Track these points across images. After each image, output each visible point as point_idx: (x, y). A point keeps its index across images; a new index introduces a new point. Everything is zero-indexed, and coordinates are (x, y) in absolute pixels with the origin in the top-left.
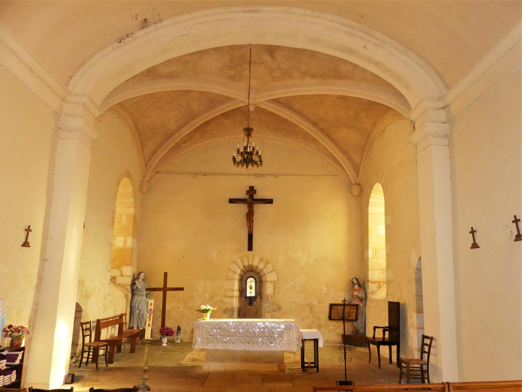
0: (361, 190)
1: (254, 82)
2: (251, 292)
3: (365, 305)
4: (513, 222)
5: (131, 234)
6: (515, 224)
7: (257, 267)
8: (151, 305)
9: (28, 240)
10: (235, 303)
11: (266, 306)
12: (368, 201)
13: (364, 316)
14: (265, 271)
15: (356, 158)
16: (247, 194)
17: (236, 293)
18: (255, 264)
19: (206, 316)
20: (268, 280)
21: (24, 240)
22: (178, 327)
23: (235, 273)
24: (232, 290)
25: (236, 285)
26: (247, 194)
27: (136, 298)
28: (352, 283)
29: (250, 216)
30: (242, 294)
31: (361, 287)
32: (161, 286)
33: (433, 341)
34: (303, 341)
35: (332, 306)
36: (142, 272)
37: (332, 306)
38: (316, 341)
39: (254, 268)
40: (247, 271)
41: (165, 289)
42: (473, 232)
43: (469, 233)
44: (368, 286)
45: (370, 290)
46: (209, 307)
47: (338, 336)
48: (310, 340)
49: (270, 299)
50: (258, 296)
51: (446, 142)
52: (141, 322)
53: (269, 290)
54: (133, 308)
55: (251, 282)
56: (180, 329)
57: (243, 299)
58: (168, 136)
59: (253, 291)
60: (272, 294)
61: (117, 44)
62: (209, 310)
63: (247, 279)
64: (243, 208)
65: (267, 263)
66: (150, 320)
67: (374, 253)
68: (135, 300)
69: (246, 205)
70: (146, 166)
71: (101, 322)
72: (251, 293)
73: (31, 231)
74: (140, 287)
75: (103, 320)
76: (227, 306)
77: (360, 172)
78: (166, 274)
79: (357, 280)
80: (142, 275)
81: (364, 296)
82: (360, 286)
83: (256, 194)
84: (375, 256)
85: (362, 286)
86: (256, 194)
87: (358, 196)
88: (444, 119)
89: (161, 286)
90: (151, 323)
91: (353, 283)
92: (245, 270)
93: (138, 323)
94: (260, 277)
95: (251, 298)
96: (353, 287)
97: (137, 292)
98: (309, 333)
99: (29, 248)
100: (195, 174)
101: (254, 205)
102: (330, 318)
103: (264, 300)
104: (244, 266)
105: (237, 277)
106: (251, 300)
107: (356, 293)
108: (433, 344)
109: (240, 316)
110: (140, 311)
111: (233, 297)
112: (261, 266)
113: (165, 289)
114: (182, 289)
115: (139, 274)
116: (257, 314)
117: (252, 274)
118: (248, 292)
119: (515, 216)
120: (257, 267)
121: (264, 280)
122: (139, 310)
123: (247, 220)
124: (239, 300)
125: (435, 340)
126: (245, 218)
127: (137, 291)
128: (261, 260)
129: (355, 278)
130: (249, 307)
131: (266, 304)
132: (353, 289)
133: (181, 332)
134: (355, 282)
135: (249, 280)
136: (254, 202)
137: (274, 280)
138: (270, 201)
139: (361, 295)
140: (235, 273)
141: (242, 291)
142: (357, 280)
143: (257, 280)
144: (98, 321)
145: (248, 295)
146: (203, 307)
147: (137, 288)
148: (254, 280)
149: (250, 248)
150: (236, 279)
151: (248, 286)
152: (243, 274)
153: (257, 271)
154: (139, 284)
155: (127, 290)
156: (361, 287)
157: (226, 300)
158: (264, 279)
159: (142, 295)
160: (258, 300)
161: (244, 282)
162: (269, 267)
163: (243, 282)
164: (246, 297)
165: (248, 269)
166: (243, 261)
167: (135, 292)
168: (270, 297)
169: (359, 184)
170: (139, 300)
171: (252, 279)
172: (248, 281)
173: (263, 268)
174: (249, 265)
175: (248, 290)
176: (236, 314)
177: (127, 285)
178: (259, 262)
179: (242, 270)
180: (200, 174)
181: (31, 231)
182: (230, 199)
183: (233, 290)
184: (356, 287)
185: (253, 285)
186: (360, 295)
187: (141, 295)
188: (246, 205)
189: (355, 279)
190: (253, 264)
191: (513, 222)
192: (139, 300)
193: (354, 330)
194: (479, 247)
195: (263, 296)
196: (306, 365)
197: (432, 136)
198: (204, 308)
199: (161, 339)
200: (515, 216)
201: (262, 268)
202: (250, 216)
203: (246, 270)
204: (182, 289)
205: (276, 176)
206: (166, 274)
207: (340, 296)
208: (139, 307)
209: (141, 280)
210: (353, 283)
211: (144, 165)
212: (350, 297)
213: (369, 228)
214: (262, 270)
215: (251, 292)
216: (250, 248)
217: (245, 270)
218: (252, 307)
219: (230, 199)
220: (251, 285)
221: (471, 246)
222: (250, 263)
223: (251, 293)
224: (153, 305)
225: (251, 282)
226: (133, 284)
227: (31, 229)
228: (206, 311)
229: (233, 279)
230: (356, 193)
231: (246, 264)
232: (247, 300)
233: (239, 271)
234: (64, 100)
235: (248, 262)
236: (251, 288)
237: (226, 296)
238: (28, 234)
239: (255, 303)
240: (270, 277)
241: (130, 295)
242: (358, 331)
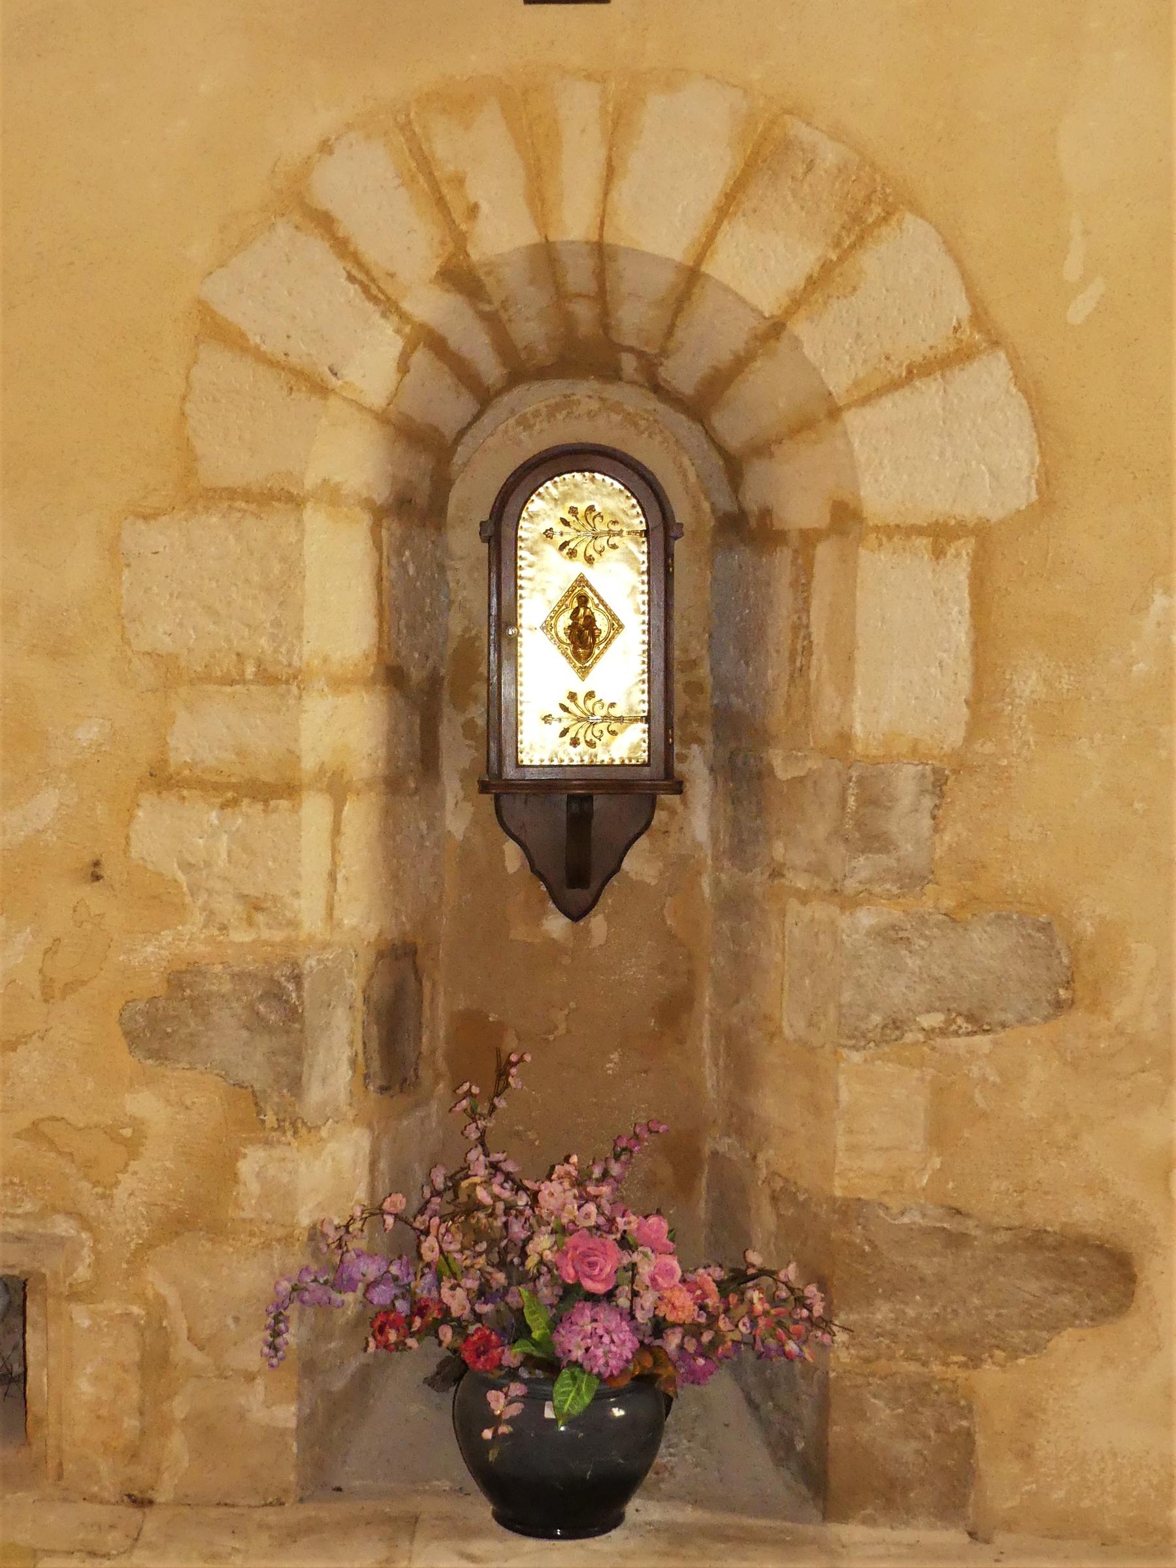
24: (268, 678)
130: (556, 924)
143: (682, 512)
150: (331, 495)
172: (528, 530)
201: (769, 303)
203: (503, 345)
218: (597, 923)
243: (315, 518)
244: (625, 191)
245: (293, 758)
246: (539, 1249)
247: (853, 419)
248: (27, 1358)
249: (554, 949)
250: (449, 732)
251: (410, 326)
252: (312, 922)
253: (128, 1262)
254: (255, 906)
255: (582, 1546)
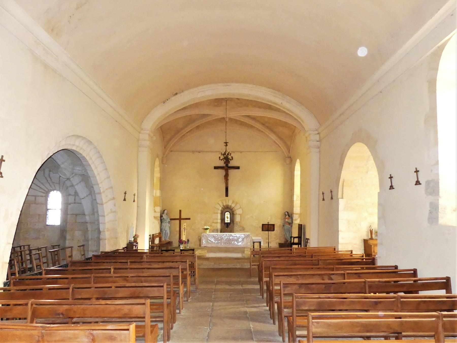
0: (291, 160)
1: (228, 107)
2: (227, 220)
3: (292, 227)
4: (389, 178)
5: (159, 188)
6: (390, 179)
7: (231, 206)
8: (185, 226)
9: (126, 198)
10: (219, 226)
11: (236, 228)
12: (295, 167)
13: (291, 233)
14: (236, 208)
15: (289, 143)
16: (224, 164)
17: (219, 221)
18: (230, 204)
19: (207, 231)
20: (237, 213)
21: (124, 198)
22: (188, 240)
23: (219, 209)
24: (217, 219)
25: (219, 216)
26: (224, 164)
27: (163, 224)
28: (285, 215)
29: (226, 177)
30: (222, 221)
31: (290, 217)
32: (178, 217)
33: (309, 240)
34: (254, 243)
35: (263, 225)
36: (165, 210)
37: (263, 225)
38: (260, 243)
39: (229, 207)
40: (225, 208)
41: (180, 219)
42: (417, 171)
43: (414, 172)
44: (293, 216)
45: (294, 219)
46: (208, 227)
47: (277, 244)
48: (257, 242)
49: (238, 224)
50: (232, 222)
51: (318, 150)
52: (167, 237)
53: (238, 219)
54: (162, 229)
55: (227, 215)
56: (189, 241)
57: (223, 224)
58: (178, 131)
59: (229, 220)
60: (240, 221)
61: (162, 104)
62: (208, 228)
63: (225, 213)
64: (222, 172)
65: (237, 204)
66: (185, 232)
67: (297, 198)
68: (163, 226)
69: (224, 170)
70: (165, 148)
71: (155, 235)
72: (227, 220)
73: (4, 161)
74: (165, 218)
75: (155, 234)
76: (214, 228)
77: (291, 150)
78: (180, 211)
79: (288, 213)
80: (166, 211)
81: (291, 222)
82: (289, 216)
83: (229, 163)
84: (297, 199)
85: (291, 216)
86: (229, 163)
87: (289, 164)
88: (318, 139)
89: (178, 217)
90: (185, 233)
91: (285, 214)
92: (224, 208)
93: (165, 238)
94: (233, 212)
95: (227, 223)
96: (286, 216)
97: (164, 221)
98: (256, 239)
99: (2, 178)
100: (193, 152)
101: (229, 170)
102: (263, 230)
103: (235, 225)
104: (223, 206)
105: (220, 212)
106: (228, 225)
107: (287, 220)
108: (308, 241)
109: (221, 232)
110: (166, 231)
111: (217, 223)
112: (233, 205)
113: (180, 219)
114: (189, 219)
115: (164, 211)
116: (232, 231)
117: (228, 210)
118: (226, 220)
119: (390, 175)
120: (231, 206)
121: (235, 213)
122: (165, 231)
123: (225, 179)
124: (221, 224)
125: (309, 240)
126: (224, 178)
127: (164, 220)
128: (233, 202)
129: (287, 212)
130: (227, 228)
131: (236, 226)
132: (285, 218)
133: (189, 242)
134: (287, 214)
135: (226, 213)
136: (229, 169)
137: (240, 213)
138: (238, 168)
139: (290, 221)
140: (219, 209)
141: (223, 219)
142: (288, 213)
143: (231, 213)
144: (153, 235)
145: (226, 222)
146: (206, 227)
147: (164, 218)
148: (229, 213)
149: (227, 195)
150: (219, 213)
151: (226, 217)
152: (223, 210)
153: (231, 209)
154: (164, 216)
155: (158, 220)
156: (290, 217)
157: (213, 225)
158: (235, 213)
159: (167, 222)
160: (232, 224)
161: (223, 214)
162: (238, 206)
163: (223, 214)
164: (225, 223)
165: (226, 207)
166: (222, 203)
167: (162, 221)
168: (238, 222)
169: (290, 157)
170: (165, 226)
171: (228, 213)
172: (225, 214)
173: (234, 206)
174: (226, 205)
175: (226, 219)
176: (219, 231)
177: (158, 217)
178: (232, 203)
179: (222, 208)
180: (197, 151)
181: (4, 161)
182: (214, 167)
183: (217, 219)
184: (287, 216)
185: (229, 216)
186: (289, 221)
187: (166, 223)
188: (224, 170)
189: (286, 212)
190: (229, 204)
191: (389, 178)
192: (165, 226)
193: (285, 241)
194: (420, 184)
195: (235, 222)
196: (279, 285)
197: (312, 148)
198: (206, 228)
199: (179, 245)
200: (390, 175)
201: (234, 207)
202: (226, 177)
203: (225, 208)
204: (189, 219)
205: (241, 152)
206: (180, 211)
207: (278, 222)
208: (165, 229)
209: (165, 214)
210: (285, 214)
211: (164, 148)
212: (284, 222)
213: (295, 184)
214: (234, 207)
215: (227, 220)
216: (227, 195)
217: (224, 208)
218: (228, 229)
219: (214, 167)
220: (227, 216)
221: (415, 183)
222: (227, 204)
223: (227, 220)
224: (186, 226)
225: (227, 215)
226: (161, 216)
227: (4, 159)
228: (207, 229)
229: (217, 213)
230: (288, 162)
231: (225, 204)
232: (225, 224)
233: (220, 209)
234: (140, 133)
235: (226, 203)
236: (228, 218)
237: (213, 223)
238: (125, 195)
239: (230, 226)
240: (238, 212)
241: (160, 223)
242: (287, 241)
243: (218, 214)
244: (229, 203)
245: (218, 222)
246: (204, 234)
247: (237, 211)
248: (354, 338)
249: (226, 229)
250: (223, 221)
251: (61, 315)
252: (218, 228)
253: (219, 244)
254: (216, 227)
255: (406, 339)
